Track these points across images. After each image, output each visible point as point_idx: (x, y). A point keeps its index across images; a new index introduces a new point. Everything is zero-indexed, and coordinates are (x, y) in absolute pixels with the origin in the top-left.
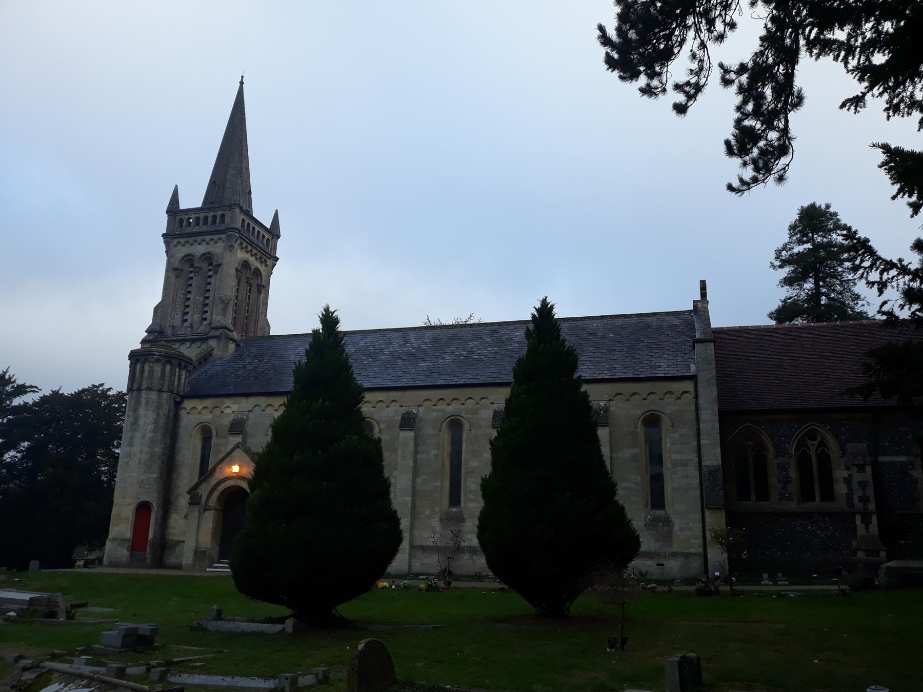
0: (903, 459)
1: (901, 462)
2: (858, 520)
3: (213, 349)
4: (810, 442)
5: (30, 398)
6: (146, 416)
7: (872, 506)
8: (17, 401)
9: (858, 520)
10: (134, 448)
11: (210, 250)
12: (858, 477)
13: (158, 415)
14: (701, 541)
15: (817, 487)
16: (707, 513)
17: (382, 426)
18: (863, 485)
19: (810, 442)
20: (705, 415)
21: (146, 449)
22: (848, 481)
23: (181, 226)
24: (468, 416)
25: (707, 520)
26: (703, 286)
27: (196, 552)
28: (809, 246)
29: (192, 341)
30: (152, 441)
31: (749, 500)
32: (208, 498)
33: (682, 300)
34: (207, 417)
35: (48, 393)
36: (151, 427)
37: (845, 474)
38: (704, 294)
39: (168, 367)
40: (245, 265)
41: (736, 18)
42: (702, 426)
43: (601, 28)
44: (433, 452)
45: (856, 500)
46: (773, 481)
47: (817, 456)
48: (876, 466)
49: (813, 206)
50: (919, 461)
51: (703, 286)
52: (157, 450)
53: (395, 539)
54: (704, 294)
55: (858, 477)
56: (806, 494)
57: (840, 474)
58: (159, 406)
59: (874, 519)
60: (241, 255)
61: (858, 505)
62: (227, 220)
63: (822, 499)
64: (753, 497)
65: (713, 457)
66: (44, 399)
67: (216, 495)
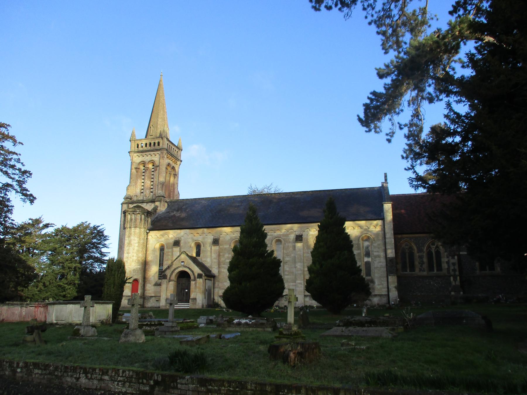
2: (452, 278)
4: (432, 246)
5: (50, 230)
7: (457, 273)
8: (43, 232)
9: (452, 278)
10: (130, 255)
12: (452, 261)
14: (387, 289)
15: (435, 265)
16: (390, 277)
18: (454, 264)
19: (432, 246)
20: (388, 236)
21: (135, 255)
22: (448, 263)
23: (138, 147)
25: (390, 280)
26: (386, 176)
29: (147, 203)
30: (138, 251)
31: (407, 271)
32: (170, 276)
33: (376, 183)
35: (60, 227)
36: (137, 245)
37: (446, 260)
38: (386, 180)
39: (133, 216)
40: (169, 165)
41: (403, 108)
42: (387, 240)
43: (358, 116)
45: (451, 271)
46: (417, 263)
47: (435, 252)
51: (386, 176)
53: (283, 288)
54: (386, 180)
55: (452, 261)
56: (431, 268)
57: (444, 260)
58: (140, 235)
59: (458, 278)
60: (167, 161)
61: (452, 273)
62: (161, 145)
63: (437, 270)
64: (408, 270)
65: (391, 253)
66: (58, 231)
67: (174, 274)
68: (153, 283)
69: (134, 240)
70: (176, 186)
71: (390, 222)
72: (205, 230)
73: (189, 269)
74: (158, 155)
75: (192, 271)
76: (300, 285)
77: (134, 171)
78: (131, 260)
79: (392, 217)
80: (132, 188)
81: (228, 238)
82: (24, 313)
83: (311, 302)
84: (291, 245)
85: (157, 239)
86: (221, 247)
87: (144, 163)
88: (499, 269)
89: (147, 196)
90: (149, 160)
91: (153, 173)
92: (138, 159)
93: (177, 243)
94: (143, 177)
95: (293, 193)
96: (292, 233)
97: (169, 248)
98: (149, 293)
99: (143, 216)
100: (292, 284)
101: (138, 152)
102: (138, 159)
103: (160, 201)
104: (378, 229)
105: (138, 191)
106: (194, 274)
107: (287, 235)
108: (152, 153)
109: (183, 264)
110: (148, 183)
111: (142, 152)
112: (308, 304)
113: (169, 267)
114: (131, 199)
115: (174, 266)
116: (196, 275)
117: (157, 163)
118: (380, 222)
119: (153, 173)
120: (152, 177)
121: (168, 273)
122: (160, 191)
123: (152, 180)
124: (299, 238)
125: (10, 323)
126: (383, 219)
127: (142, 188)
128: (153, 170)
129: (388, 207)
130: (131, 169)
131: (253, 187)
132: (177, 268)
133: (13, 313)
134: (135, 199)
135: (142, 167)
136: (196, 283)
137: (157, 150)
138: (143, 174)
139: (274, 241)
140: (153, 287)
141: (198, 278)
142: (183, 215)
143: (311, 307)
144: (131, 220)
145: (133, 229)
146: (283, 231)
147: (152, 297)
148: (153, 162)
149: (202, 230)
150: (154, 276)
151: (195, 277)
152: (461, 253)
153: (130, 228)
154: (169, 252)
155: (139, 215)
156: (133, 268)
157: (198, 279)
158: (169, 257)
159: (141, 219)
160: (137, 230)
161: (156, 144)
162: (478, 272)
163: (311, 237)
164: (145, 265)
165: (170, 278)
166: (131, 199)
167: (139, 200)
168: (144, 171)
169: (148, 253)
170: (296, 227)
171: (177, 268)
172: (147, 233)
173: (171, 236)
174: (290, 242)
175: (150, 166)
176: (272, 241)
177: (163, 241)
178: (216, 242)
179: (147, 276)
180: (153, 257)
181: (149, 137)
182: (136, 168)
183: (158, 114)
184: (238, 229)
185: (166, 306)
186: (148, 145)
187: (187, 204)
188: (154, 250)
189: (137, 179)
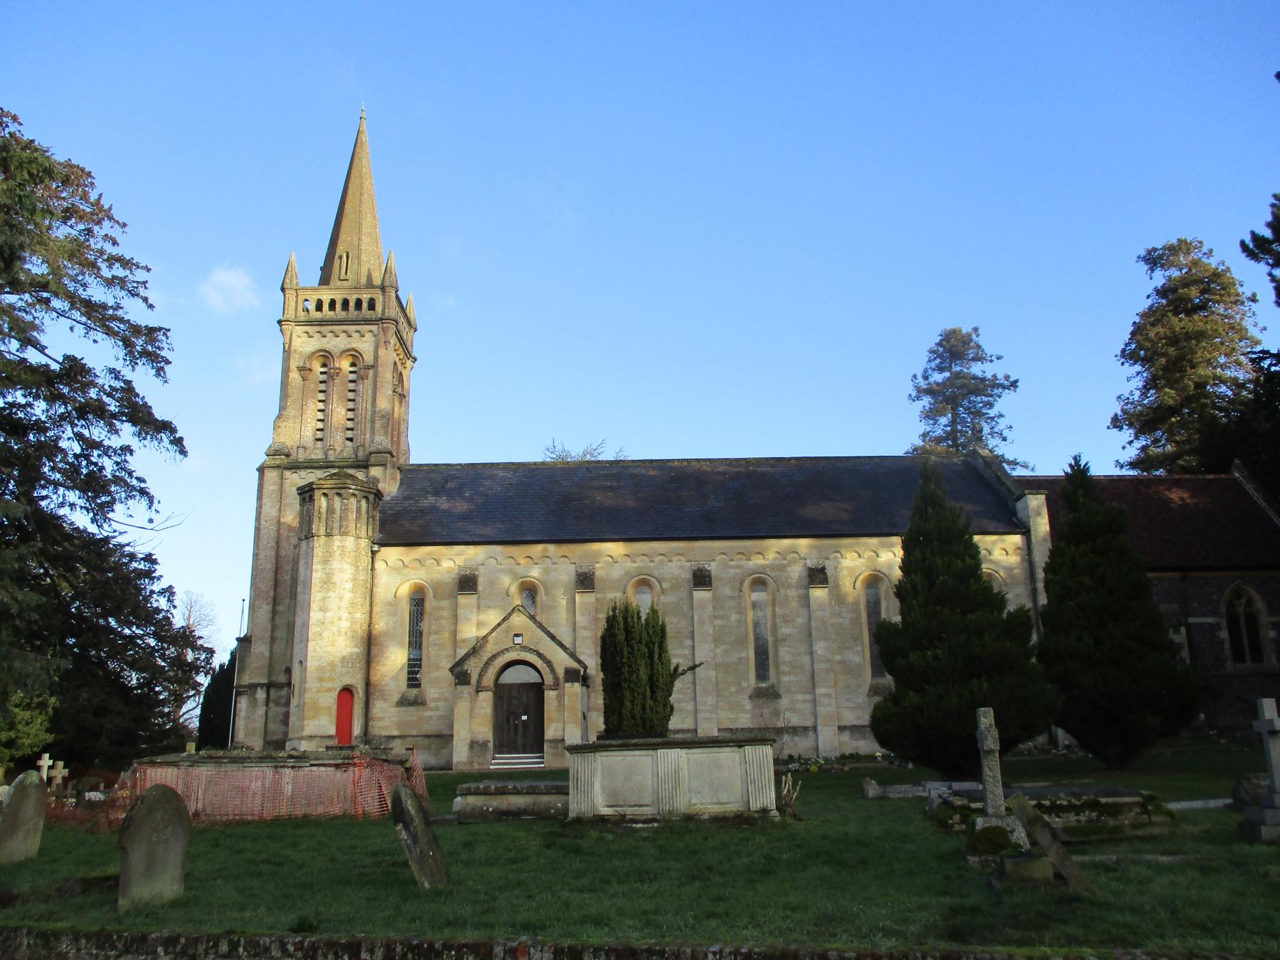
0: (1211, 620)
1: (1209, 624)
3: (378, 481)
6: (342, 571)
10: (329, 614)
11: (354, 345)
13: (357, 567)
17: (665, 585)
21: (345, 615)
24: (773, 574)
27: (473, 745)
28: (947, 374)
30: (353, 604)
32: (481, 676)
34: (535, 573)
36: (349, 586)
39: (337, 502)
44: (734, 617)
48: (1188, 626)
49: (954, 332)
50: (1224, 622)
52: (358, 616)
62: (379, 308)
68: (396, 698)
69: (342, 571)
70: (403, 427)
71: (1044, 540)
72: (552, 548)
73: (540, 655)
74: (369, 336)
75: (549, 663)
76: (826, 701)
77: (295, 376)
78: (335, 629)
79: (1048, 528)
80: (290, 423)
81: (617, 572)
82: (288, 789)
83: (854, 743)
84: (793, 593)
85: (401, 571)
86: (599, 596)
87: (326, 357)
88: (1274, 658)
89: (339, 449)
90: (342, 347)
91: (351, 386)
92: (305, 343)
93: (467, 583)
94: (321, 396)
95: (747, 461)
96: (794, 561)
97: (443, 599)
98: (382, 728)
99: (364, 502)
100: (800, 697)
101: (310, 323)
102: (305, 343)
103: (384, 465)
104: (1014, 559)
105: (309, 433)
106: (553, 670)
107: (782, 568)
108: (352, 328)
109: (518, 640)
110: (339, 413)
111: (321, 323)
112: (848, 751)
113: (474, 651)
114: (288, 455)
115: (490, 649)
116: (561, 672)
117: (368, 358)
118: (1016, 539)
119: (351, 386)
120: (351, 395)
121: (473, 667)
122: (379, 438)
123: (351, 405)
124: (817, 576)
125: (228, 824)
126: (1025, 530)
127: (320, 425)
128: (352, 377)
129: (1036, 502)
130: (286, 371)
131: (559, 447)
132: (502, 652)
133: (243, 791)
134: (302, 456)
135: (317, 368)
136: (560, 698)
137: (368, 322)
138: (322, 387)
139: (747, 583)
140: (394, 710)
141: (567, 680)
142: (461, 506)
143: (872, 758)
144: (330, 510)
145: (337, 541)
146: (771, 556)
147: (394, 737)
148: (355, 357)
149: (540, 547)
150: (395, 678)
151: (556, 679)
152: (1191, 620)
153: (329, 535)
154: (440, 609)
155: (353, 500)
156: (340, 655)
157: (568, 685)
158: (444, 622)
159: (359, 510)
160: (350, 542)
161: (365, 305)
162: (1230, 666)
163: (845, 572)
164: (370, 645)
165: (479, 682)
166: (288, 455)
167: (311, 461)
168: (323, 377)
169: (376, 609)
170: (803, 544)
171: (502, 652)
172: (374, 553)
173: (447, 564)
174: (790, 586)
175: (345, 365)
176: (742, 583)
177: (419, 576)
178: (585, 581)
179: (375, 678)
180: (393, 623)
181: (335, 282)
182: (301, 369)
183: (360, 224)
184: (897, 540)
185: (471, 763)
186: (338, 306)
187: (453, 477)
188: (393, 604)
189: (304, 397)
